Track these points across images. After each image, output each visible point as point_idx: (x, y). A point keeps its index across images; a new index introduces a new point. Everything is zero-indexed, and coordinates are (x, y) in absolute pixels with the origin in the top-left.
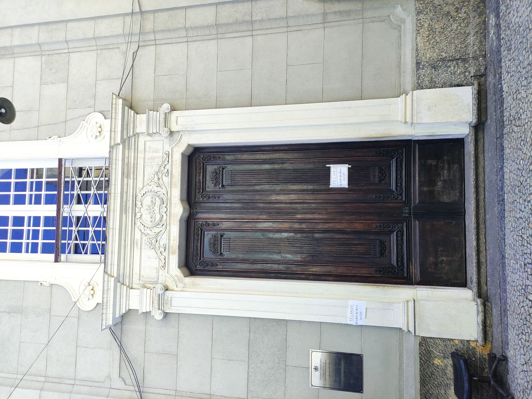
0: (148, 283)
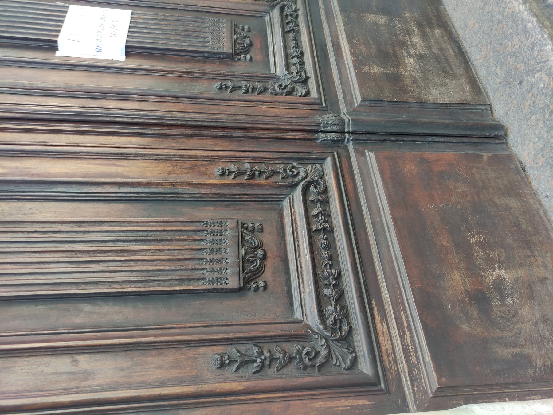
0: (320, 233)
